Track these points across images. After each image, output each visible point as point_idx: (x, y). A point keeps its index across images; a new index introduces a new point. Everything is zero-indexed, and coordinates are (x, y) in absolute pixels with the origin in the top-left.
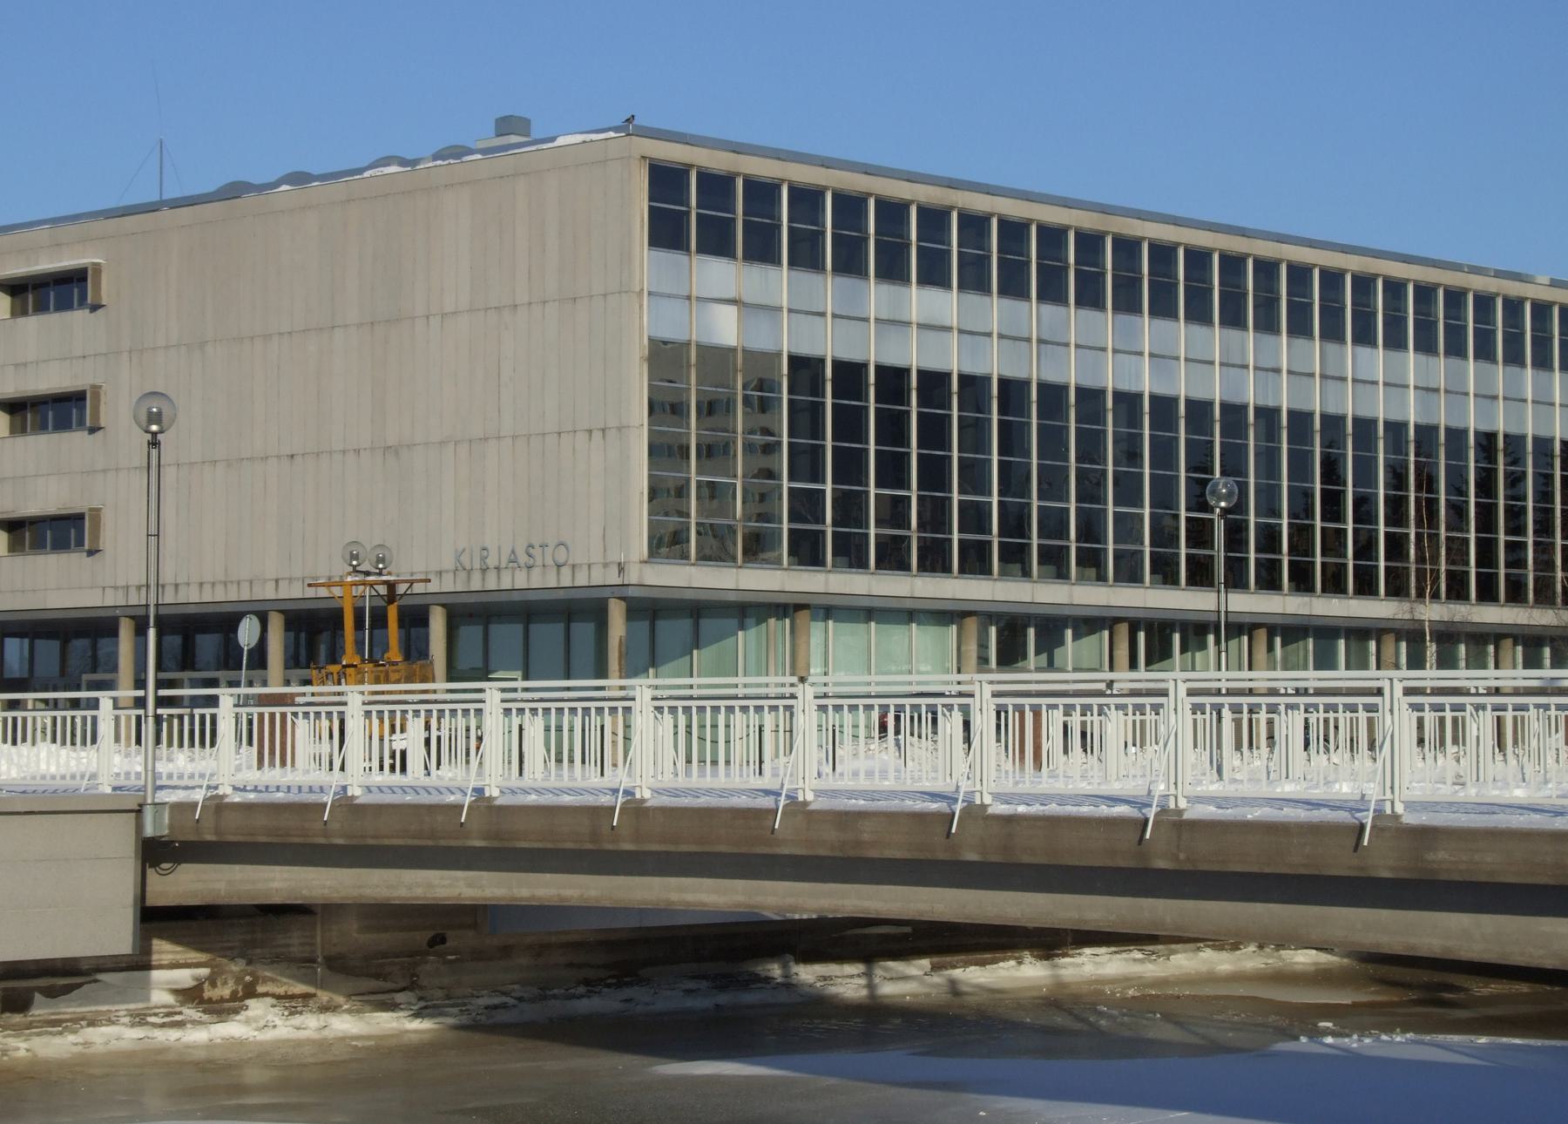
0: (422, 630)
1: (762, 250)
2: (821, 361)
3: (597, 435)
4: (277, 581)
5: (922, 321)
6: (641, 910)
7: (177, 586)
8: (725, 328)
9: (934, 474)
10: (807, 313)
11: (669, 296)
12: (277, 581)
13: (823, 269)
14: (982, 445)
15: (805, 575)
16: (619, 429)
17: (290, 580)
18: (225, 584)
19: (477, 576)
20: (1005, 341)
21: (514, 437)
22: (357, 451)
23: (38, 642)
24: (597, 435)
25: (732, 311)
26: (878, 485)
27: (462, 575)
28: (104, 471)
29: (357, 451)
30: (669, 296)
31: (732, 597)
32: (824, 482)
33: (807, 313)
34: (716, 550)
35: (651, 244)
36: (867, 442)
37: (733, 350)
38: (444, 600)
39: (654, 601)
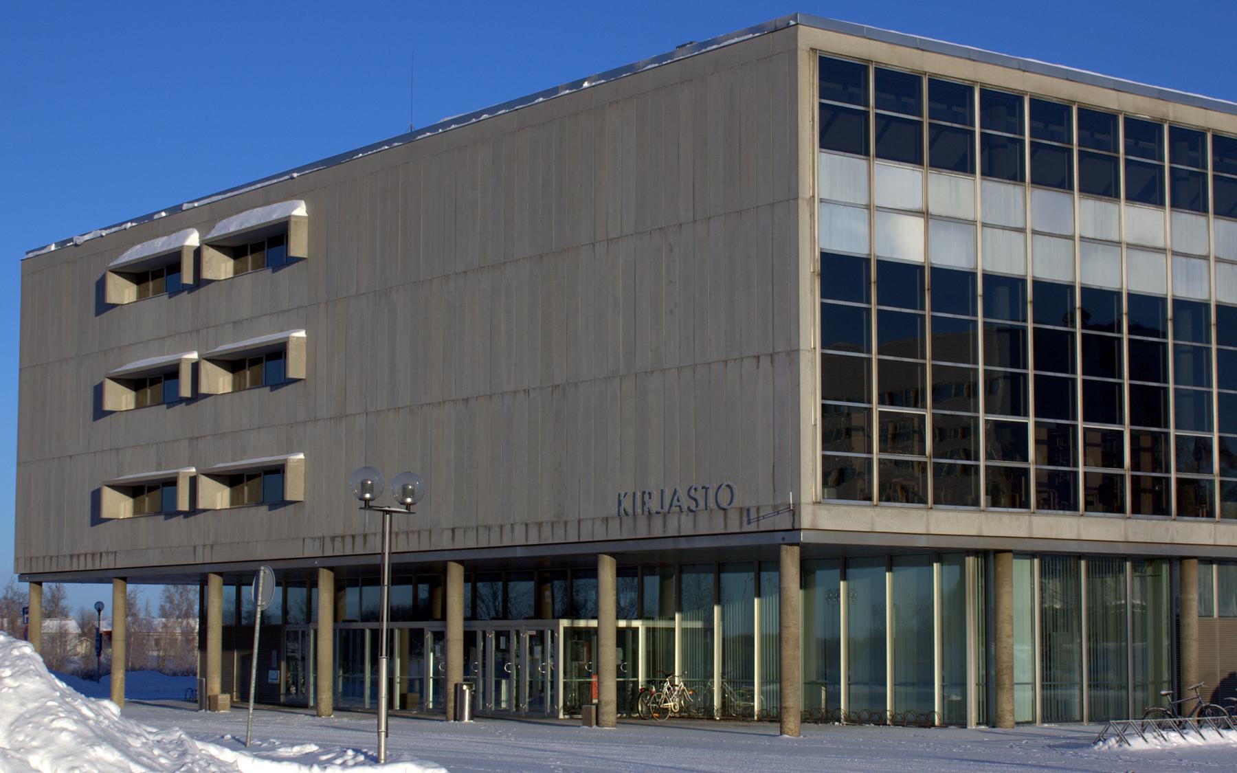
0: (592, 580)
1: (953, 158)
2: (1023, 281)
3: (765, 362)
4: (453, 530)
5: (1131, 241)
6: (1063, 509)
7: (365, 536)
8: (908, 243)
9: (1149, 407)
10: (1004, 228)
11: (845, 204)
12: (453, 530)
13: (1023, 180)
14: (1201, 376)
15: (1006, 518)
16: (788, 353)
17: (466, 529)
18: (407, 534)
19: (614, 524)
20: (1222, 266)
21: (680, 369)
22: (527, 392)
23: (290, 589)
24: (765, 362)
25: (919, 222)
26: (1086, 419)
27: (628, 521)
28: (305, 422)
29: (527, 392)
30: (845, 204)
31: (922, 543)
32: (1026, 414)
33: (1004, 228)
34: (900, 488)
35: (821, 146)
36: (1074, 371)
37: (919, 268)
38: (460, 556)
39: (845, 548)
